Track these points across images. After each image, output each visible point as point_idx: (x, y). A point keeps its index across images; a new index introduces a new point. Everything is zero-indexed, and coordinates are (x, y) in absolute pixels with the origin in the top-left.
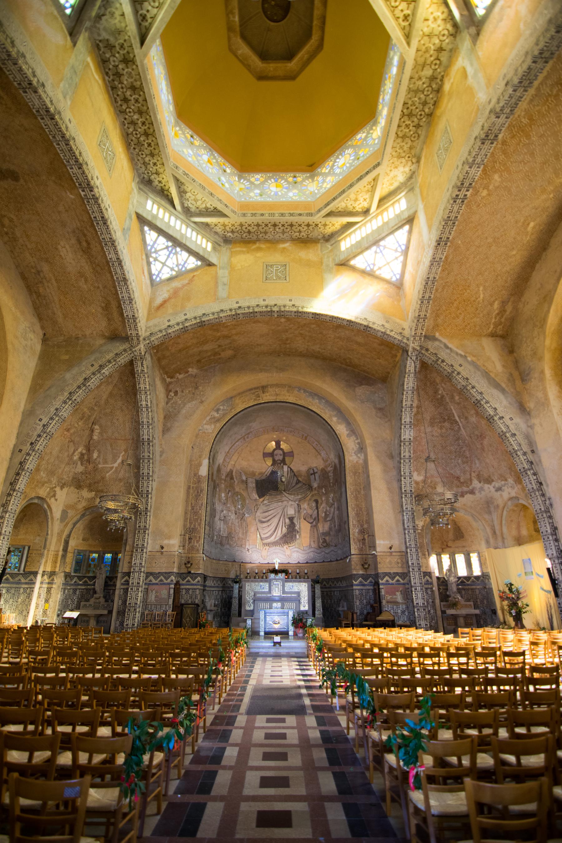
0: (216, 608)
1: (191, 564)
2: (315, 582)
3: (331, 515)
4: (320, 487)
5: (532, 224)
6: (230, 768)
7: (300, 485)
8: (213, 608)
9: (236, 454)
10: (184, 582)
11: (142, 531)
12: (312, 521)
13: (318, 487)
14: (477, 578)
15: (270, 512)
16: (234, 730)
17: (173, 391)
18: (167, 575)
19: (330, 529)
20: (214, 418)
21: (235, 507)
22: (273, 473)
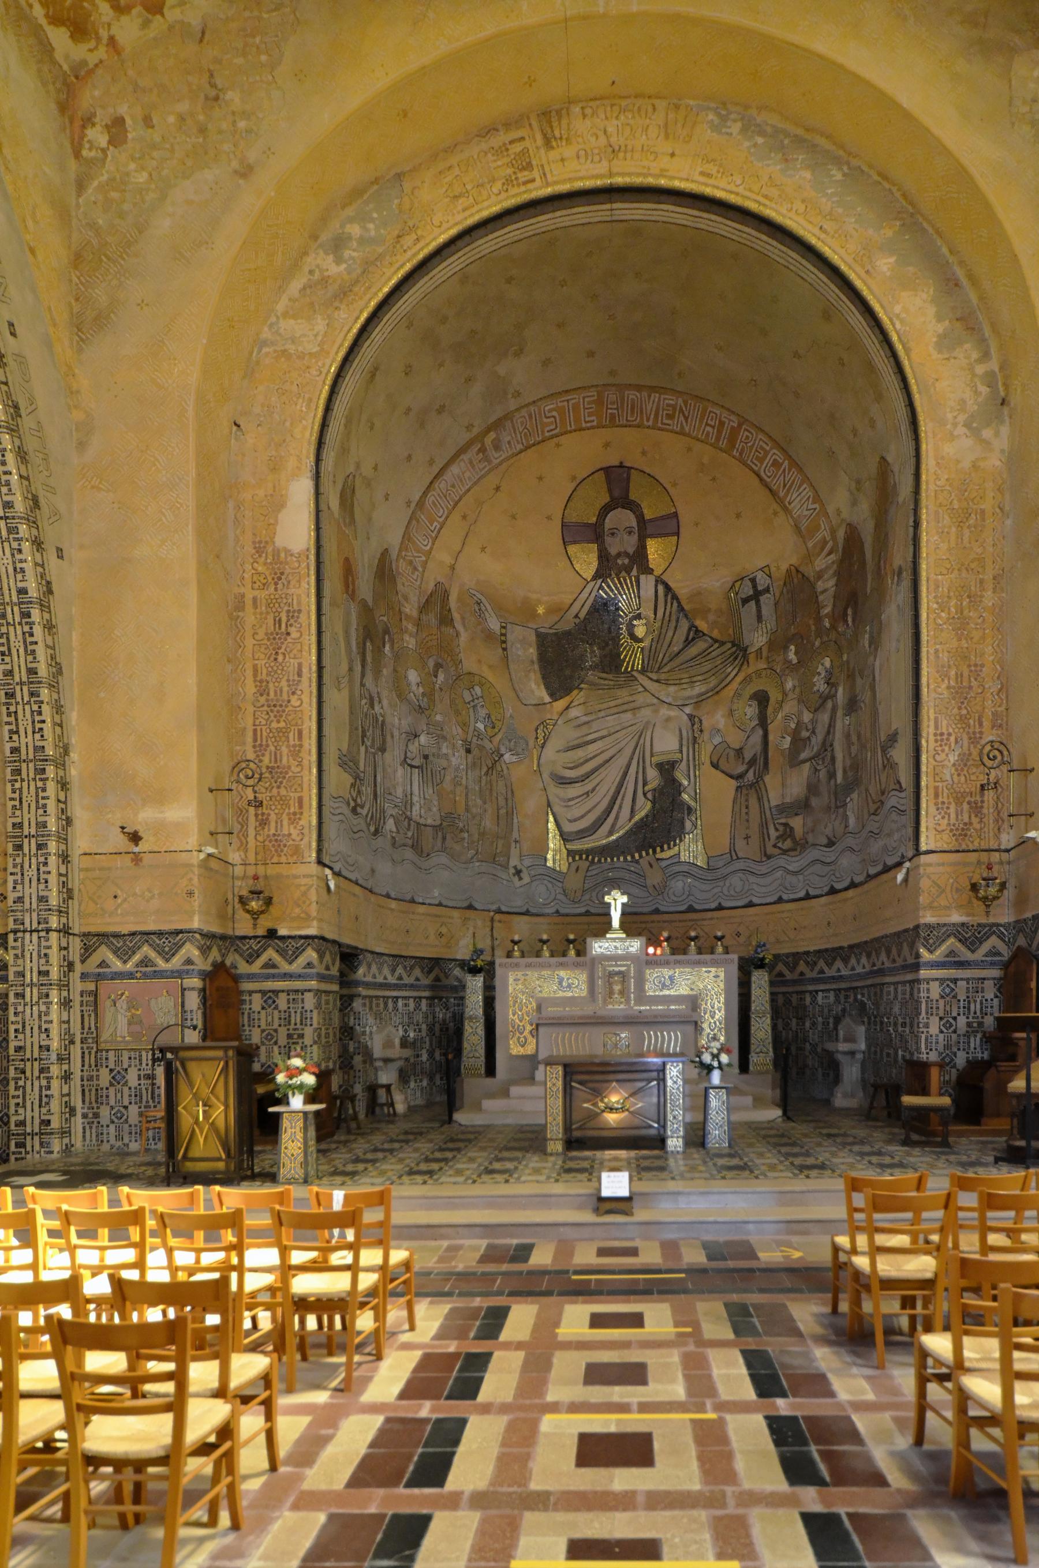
0: (407, 1053)
1: (269, 901)
2: (747, 967)
3: (817, 741)
4: (778, 644)
6: (519, 1346)
7: (700, 645)
8: (396, 1052)
9: (456, 517)
10: (256, 968)
11: (28, 770)
12: (741, 769)
13: (772, 645)
15: (592, 749)
16: (497, 1355)
17: (102, 117)
18: (169, 940)
19: (812, 789)
20: (325, 281)
21: (465, 725)
22: (602, 609)
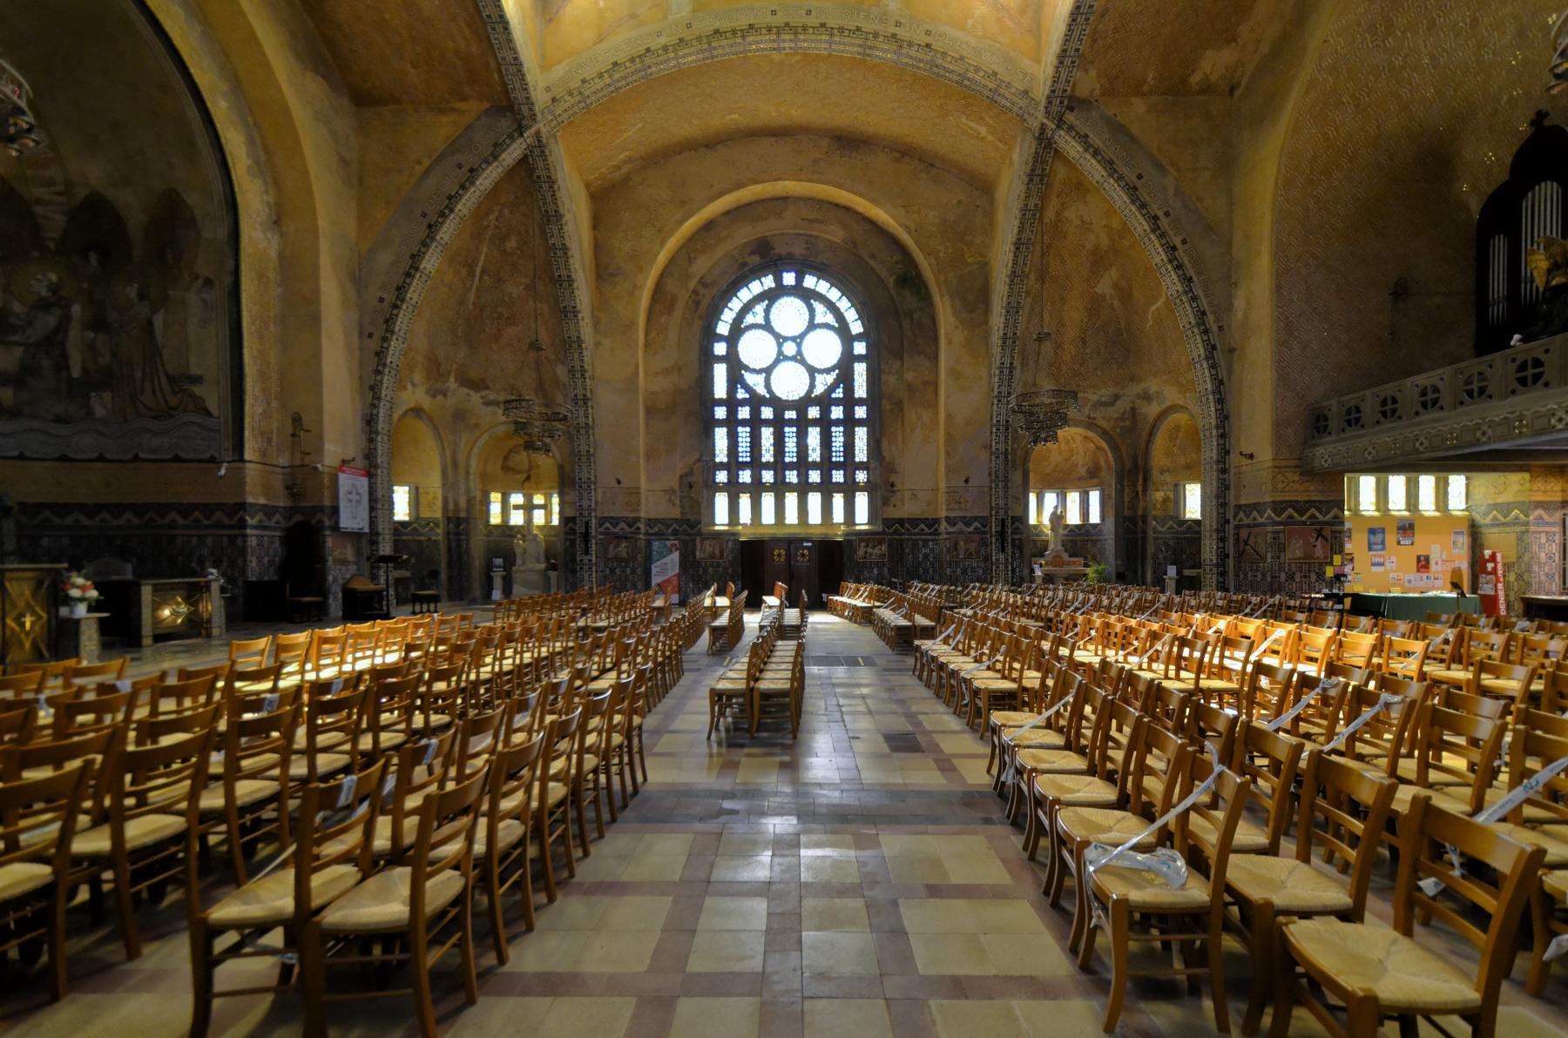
5: (735, 116)
14: (1095, 526)
